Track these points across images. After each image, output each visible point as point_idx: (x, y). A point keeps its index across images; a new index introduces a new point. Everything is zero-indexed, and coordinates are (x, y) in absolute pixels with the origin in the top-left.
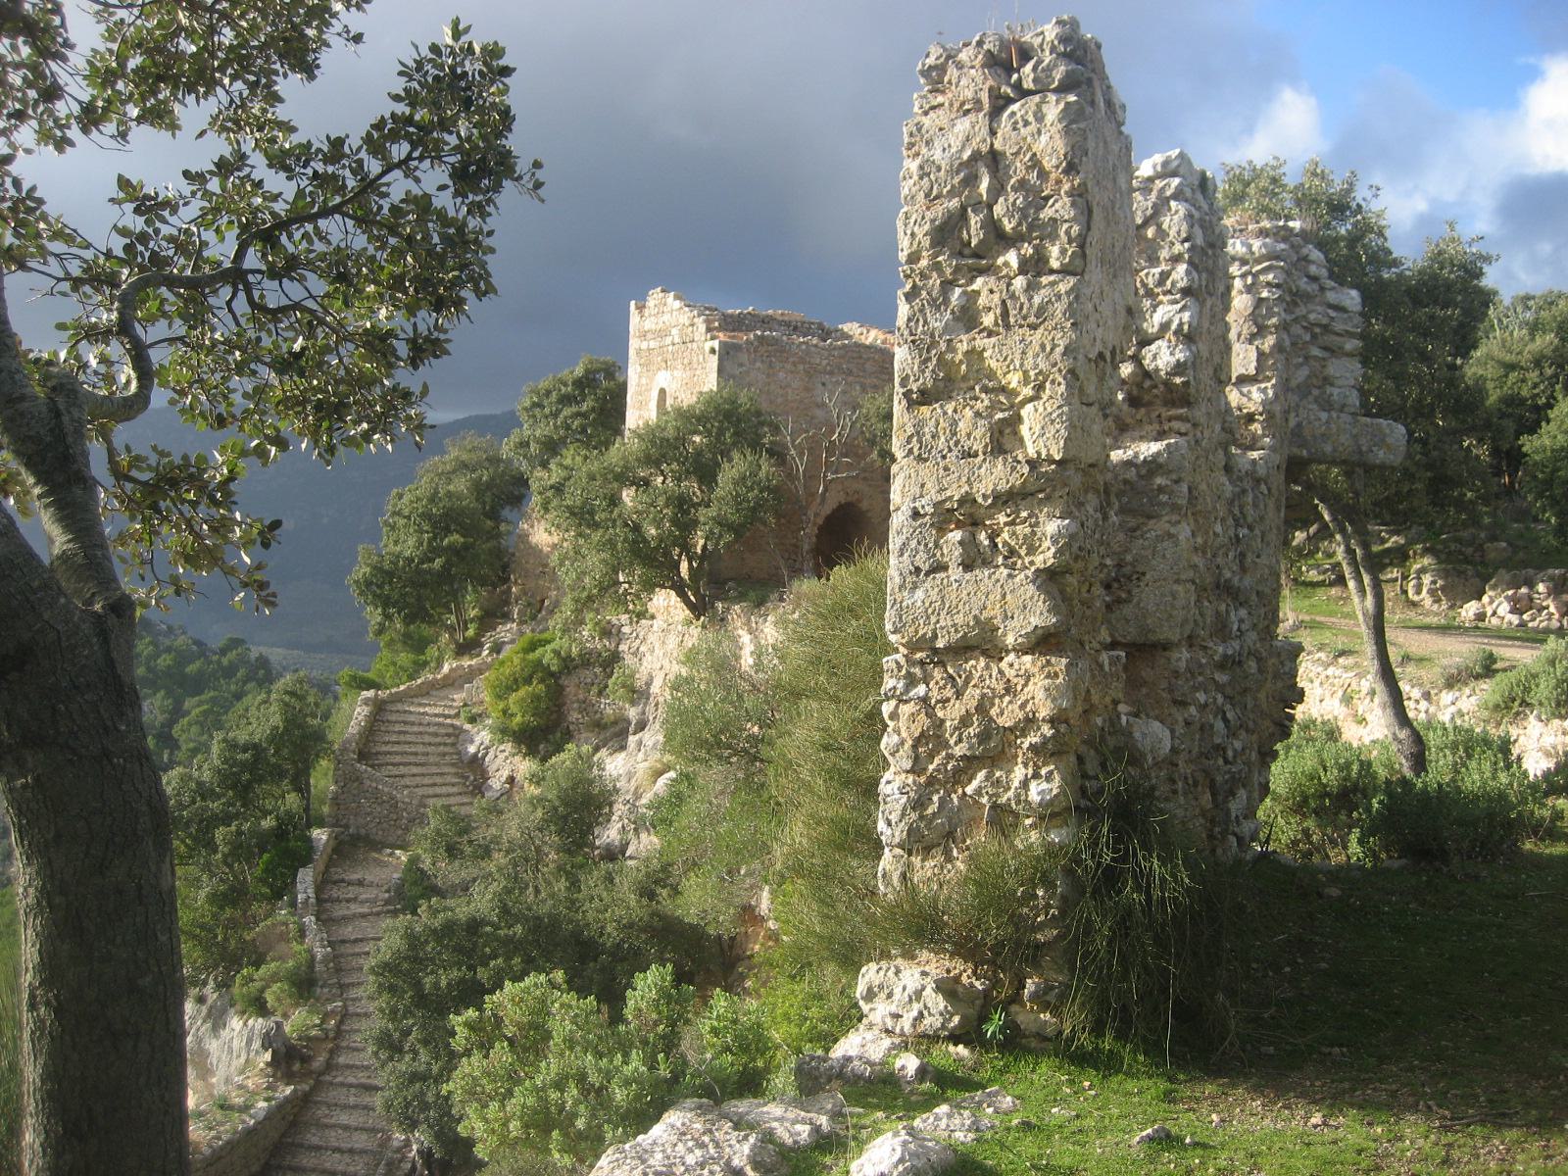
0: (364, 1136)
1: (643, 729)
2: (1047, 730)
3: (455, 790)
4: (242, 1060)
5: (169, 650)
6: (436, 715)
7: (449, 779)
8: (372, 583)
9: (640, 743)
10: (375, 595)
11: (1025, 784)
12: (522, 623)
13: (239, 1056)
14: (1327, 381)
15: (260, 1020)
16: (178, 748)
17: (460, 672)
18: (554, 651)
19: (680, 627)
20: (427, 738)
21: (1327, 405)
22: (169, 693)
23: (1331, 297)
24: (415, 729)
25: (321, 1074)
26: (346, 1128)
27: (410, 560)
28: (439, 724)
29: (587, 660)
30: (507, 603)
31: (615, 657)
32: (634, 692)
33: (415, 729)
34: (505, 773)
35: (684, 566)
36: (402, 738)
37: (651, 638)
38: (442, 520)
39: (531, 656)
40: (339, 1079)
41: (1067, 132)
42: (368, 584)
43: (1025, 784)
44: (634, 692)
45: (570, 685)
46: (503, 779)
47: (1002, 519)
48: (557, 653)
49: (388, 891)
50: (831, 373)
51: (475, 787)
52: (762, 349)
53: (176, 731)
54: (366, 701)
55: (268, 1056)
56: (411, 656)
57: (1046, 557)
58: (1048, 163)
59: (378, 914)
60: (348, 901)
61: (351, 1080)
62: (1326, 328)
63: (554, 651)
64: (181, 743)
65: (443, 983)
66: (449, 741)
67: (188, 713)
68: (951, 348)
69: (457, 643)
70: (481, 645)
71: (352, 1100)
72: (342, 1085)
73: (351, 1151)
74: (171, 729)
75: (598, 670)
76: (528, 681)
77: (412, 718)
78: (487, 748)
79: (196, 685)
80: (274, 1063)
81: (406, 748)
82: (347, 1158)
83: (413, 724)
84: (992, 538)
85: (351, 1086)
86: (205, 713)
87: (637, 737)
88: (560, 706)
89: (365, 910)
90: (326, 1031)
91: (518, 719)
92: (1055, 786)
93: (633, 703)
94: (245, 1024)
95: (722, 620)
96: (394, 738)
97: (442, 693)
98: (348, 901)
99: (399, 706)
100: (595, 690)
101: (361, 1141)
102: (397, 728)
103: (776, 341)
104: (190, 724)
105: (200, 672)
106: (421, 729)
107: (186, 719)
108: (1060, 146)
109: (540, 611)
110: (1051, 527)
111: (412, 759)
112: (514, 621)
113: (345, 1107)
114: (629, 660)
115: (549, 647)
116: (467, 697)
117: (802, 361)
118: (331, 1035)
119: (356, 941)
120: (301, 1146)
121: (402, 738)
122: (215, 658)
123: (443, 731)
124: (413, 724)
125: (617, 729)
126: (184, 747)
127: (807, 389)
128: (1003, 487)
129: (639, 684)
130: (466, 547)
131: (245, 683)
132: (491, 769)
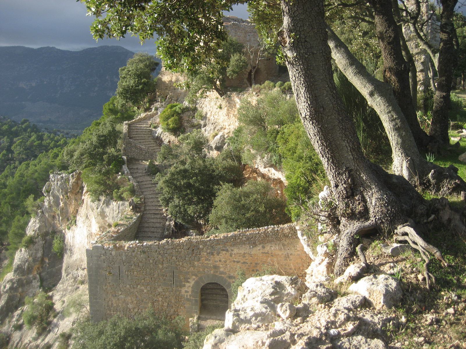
0: (158, 224)
1: (205, 126)
2: (422, 81)
3: (154, 145)
4: (117, 212)
5: (5, 124)
6: (144, 127)
7: (152, 143)
8: (123, 93)
9: (205, 130)
10: (124, 96)
11: (419, 88)
12: (161, 102)
13: (116, 211)
14: (436, 37)
15: (121, 202)
16: (14, 153)
17: (148, 116)
18: (179, 108)
19: (215, 100)
20: (144, 133)
21: (436, 41)
22: (8, 137)
23: (437, 24)
24: (140, 131)
25: (143, 211)
26: (153, 223)
27: (132, 86)
28: (146, 129)
29: (187, 109)
30: (155, 97)
31: (195, 110)
32: (202, 117)
33: (140, 131)
34: (167, 140)
35: (218, 83)
36: (137, 133)
37: (205, 103)
38: (140, 76)
39: (172, 109)
40: (148, 212)
41: (426, 8)
42: (122, 93)
43: (419, 88)
44: (202, 117)
45: (185, 117)
46: (167, 142)
47: (416, 56)
48: (180, 108)
49: (145, 170)
50: (251, 33)
51: (160, 144)
52: (233, 27)
53: (12, 148)
54: (126, 124)
55: (131, 207)
56: (114, 116)
57: (422, 60)
58: (423, 12)
59: (144, 176)
60: (136, 173)
61: (151, 212)
62: (436, 29)
63: (179, 108)
64: (15, 151)
65: (182, 183)
66: (150, 133)
67: (15, 142)
68: (410, 35)
69: (145, 108)
70: (151, 109)
71: (153, 217)
72: (149, 213)
73: (156, 227)
74: (11, 148)
75: (191, 112)
76: (173, 116)
77: (138, 128)
78: (160, 134)
79: (16, 134)
80: (133, 209)
81: (139, 135)
82: (156, 229)
83: (139, 129)
84: (415, 58)
85: (151, 214)
86: (21, 142)
87: (204, 128)
88: (181, 122)
89: (141, 175)
90: (142, 202)
91: (171, 126)
92: (423, 88)
93: (202, 120)
94: (117, 203)
95: (229, 97)
96: (135, 133)
97: (145, 121)
98: (136, 173)
99: (134, 125)
100: (191, 117)
101: (158, 225)
102: (135, 130)
103: (237, 24)
104: (17, 146)
105: (16, 130)
106: (142, 130)
107: (15, 144)
108: (425, 10)
109: (166, 99)
110: (423, 57)
111: (142, 138)
112: (159, 102)
113: (151, 218)
114: (199, 109)
115: (177, 107)
116: (156, 120)
117: (244, 29)
118: (143, 203)
119: (141, 182)
120: (144, 227)
121: (137, 133)
122: (20, 126)
123: (147, 131)
124: (139, 129)
125: (198, 127)
126: (16, 153)
127: (245, 37)
128: (417, 52)
129: (204, 114)
130: (148, 82)
131: (31, 133)
132: (163, 139)
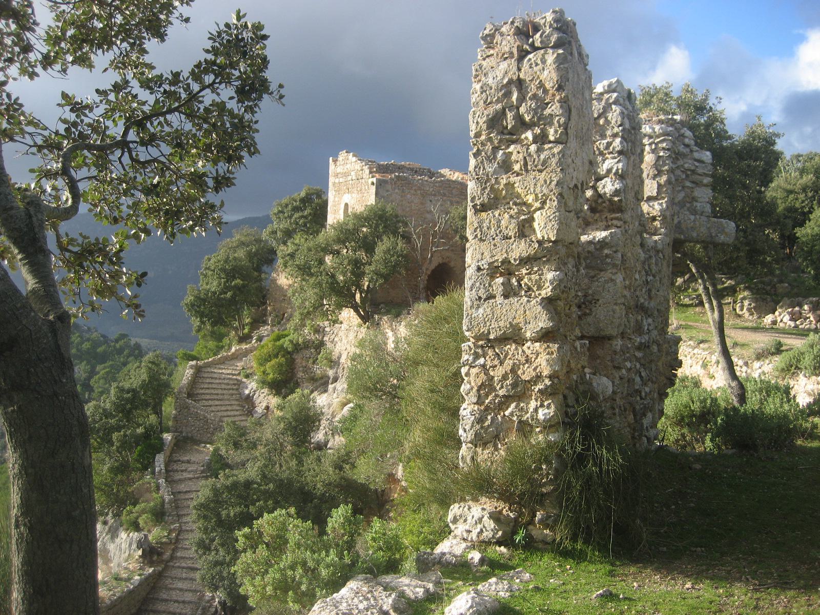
0: (191, 594)
1: (336, 381)
2: (547, 382)
3: (238, 413)
4: (127, 554)
5: (88, 340)
6: (228, 374)
7: (235, 407)
8: (194, 305)
9: (335, 389)
10: (196, 311)
11: (536, 410)
12: (273, 326)
13: (125, 552)
14: (694, 199)
15: (136, 533)
16: (93, 391)
17: (240, 352)
18: (290, 341)
19: (355, 328)
20: (223, 386)
21: (694, 212)
22: (88, 363)
23: (696, 155)
24: (217, 381)
25: (168, 561)
26: (181, 590)
27: (215, 293)
28: (230, 379)
29: (307, 345)
30: (265, 315)
31: (322, 344)
32: (332, 362)
33: (217, 381)
34: (264, 404)
35: (358, 296)
36: (210, 386)
37: (341, 334)
38: (231, 272)
39: (278, 343)
40: (177, 564)
42: (193, 305)
43: (536, 410)
44: (332, 362)
45: (298, 358)
46: (263, 407)
47: (524, 271)
48: (291, 341)
49: (203, 466)
50: (435, 195)
51: (248, 412)
52: (399, 183)
53: (92, 382)
54: (191, 367)
55: (140, 552)
56: (215, 343)
57: (547, 291)
58: (548, 85)
59: (198, 478)
60: (182, 471)
61: (184, 565)
62: (693, 172)
63: (290, 341)
64: (94, 388)
65: (232, 514)
66: (235, 387)
67: (98, 373)
69: (239, 336)
70: (252, 338)
71: (184, 575)
72: (179, 567)
73: (184, 602)
74: (89, 381)
75: (313, 350)
76: (276, 356)
77: (215, 376)
78: (255, 391)
79: (103, 358)
80: (143, 556)
81: (213, 391)
82: (181, 606)
83: (216, 378)
84: (519, 281)
85: (183, 568)
86: (107, 373)
87: (333, 385)
88: (293, 369)
89: (191, 476)
90: (170, 539)
91: (271, 376)
92: (552, 411)
93: (331, 368)
94: (128, 536)
95: (378, 324)
96: (206, 386)
97: (231, 363)
98: (182, 471)
99: (209, 369)
100: (311, 361)
101: (189, 597)
102: (208, 381)
103: (406, 178)
104: (99, 379)
105: (105, 352)
106: (220, 381)
107: (97, 376)
108: (555, 76)
109: (282, 320)
110: (550, 276)
111: (215, 397)
112: (269, 325)
113: (181, 579)
114: (329, 345)
115: (287, 339)
116: (244, 365)
117: (420, 189)
118: (173, 541)
119: (186, 492)
120: (158, 599)
121: (210, 386)
122: (113, 344)
123: (231, 382)
124: (216, 378)
125: (323, 381)
126: (96, 391)
127: (422, 204)
128: (524, 255)
129: (334, 357)
130: (244, 286)
131: (128, 357)
132: (257, 402)
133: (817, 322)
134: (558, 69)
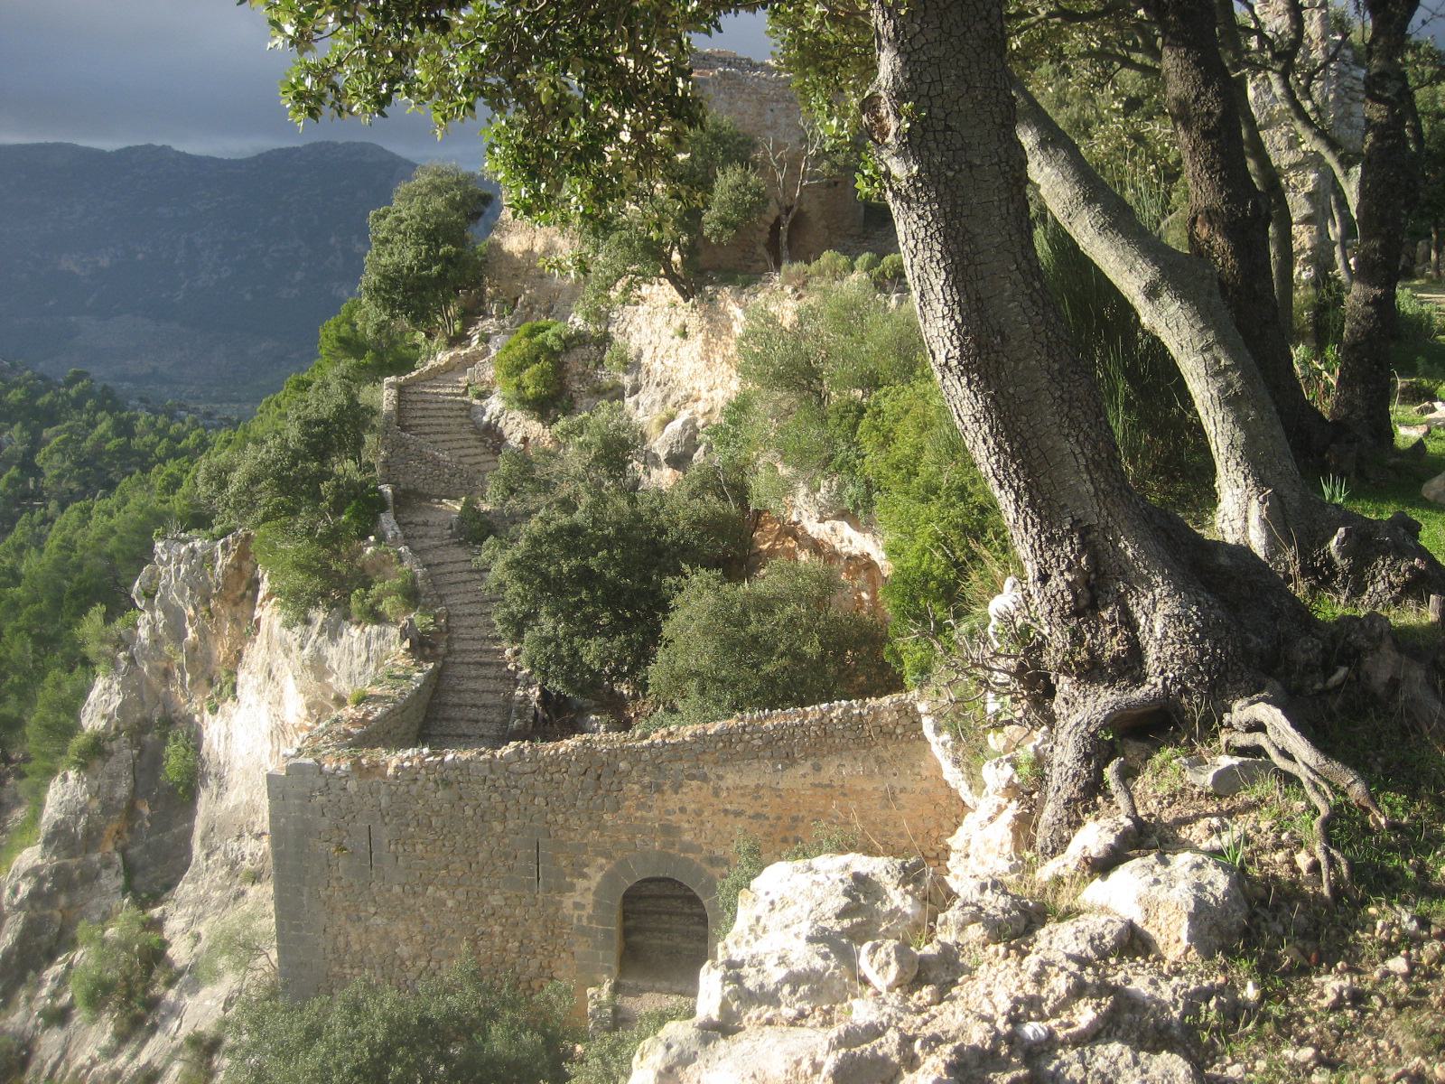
0: (491, 696)
1: (637, 392)
2: (1309, 253)
3: (478, 451)
4: (363, 658)
5: (17, 385)
6: (448, 394)
7: (472, 443)
8: (380, 289)
9: (637, 404)
10: (384, 299)
11: (1300, 273)
12: (501, 317)
13: (359, 656)
14: (1351, 114)
15: (376, 627)
16: (43, 475)
17: (458, 360)
18: (555, 335)
19: (666, 309)
20: (446, 413)
21: (1350, 126)
22: (25, 426)
23: (1354, 73)
24: (435, 406)
25: (445, 656)
26: (475, 691)
27: (410, 269)
28: (451, 401)
29: (580, 339)
30: (482, 302)
31: (605, 340)
32: (626, 363)
33: (435, 406)
34: (519, 436)
35: (676, 257)
36: (425, 413)
37: (637, 320)
38: (433, 235)
39: (535, 340)
40: (459, 660)
42: (377, 290)
43: (1300, 273)
44: (626, 363)
45: (574, 363)
46: (518, 440)
47: (1291, 174)
48: (558, 336)
49: (451, 527)
50: (777, 101)
51: (495, 448)
52: (724, 83)
53: (38, 459)
54: (391, 385)
55: (407, 644)
56: (353, 361)
57: (1309, 187)
58: (1313, 37)
59: (447, 545)
60: (421, 537)
61: (467, 660)
62: (1352, 89)
63: (555, 335)
64: (45, 470)
65: (565, 569)
66: (464, 413)
67: (48, 442)
69: (448, 337)
70: (469, 338)
71: (473, 673)
72: (462, 663)
73: (484, 706)
74: (33, 458)
75: (593, 348)
76: (536, 359)
77: (429, 398)
78: (498, 417)
79: (50, 417)
80: (412, 649)
81: (431, 421)
82: (483, 711)
83: (431, 402)
84: (1287, 181)
85: (469, 663)
86: (65, 442)
87: (633, 399)
88: (562, 379)
89: (436, 542)
90: (440, 627)
91: (531, 390)
92: (1312, 273)
93: (626, 372)
94: (363, 631)
95: (711, 300)
96: (420, 413)
97: (449, 376)
98: (421, 537)
99: (415, 389)
100: (592, 364)
101: (489, 699)
102: (419, 405)
103: (735, 76)
104: (51, 452)
105: (51, 403)
106: (439, 405)
107: (47, 449)
108: (1319, 31)
109: (514, 307)
110: (1312, 176)
111: (439, 429)
112: (492, 316)
113: (470, 678)
114: (618, 339)
115: (549, 332)
116: (484, 374)
117: (756, 92)
118: (444, 629)
119: (438, 565)
120: (446, 704)
121: (425, 413)
122: (63, 390)
123: (456, 406)
124: (431, 402)
125: (614, 394)
126: (49, 474)
127: (760, 115)
128: (1293, 161)
129: (632, 354)
130: (458, 255)
131: (96, 413)
132: (506, 432)
133: (15, 725)
134: (1323, 25)
